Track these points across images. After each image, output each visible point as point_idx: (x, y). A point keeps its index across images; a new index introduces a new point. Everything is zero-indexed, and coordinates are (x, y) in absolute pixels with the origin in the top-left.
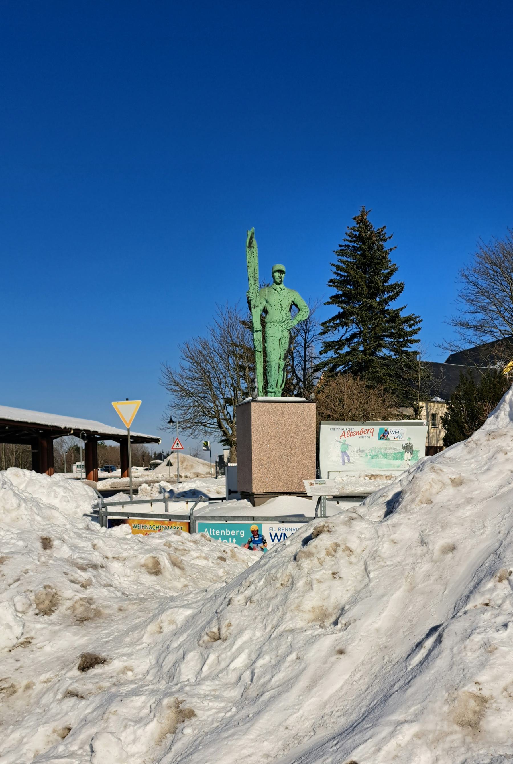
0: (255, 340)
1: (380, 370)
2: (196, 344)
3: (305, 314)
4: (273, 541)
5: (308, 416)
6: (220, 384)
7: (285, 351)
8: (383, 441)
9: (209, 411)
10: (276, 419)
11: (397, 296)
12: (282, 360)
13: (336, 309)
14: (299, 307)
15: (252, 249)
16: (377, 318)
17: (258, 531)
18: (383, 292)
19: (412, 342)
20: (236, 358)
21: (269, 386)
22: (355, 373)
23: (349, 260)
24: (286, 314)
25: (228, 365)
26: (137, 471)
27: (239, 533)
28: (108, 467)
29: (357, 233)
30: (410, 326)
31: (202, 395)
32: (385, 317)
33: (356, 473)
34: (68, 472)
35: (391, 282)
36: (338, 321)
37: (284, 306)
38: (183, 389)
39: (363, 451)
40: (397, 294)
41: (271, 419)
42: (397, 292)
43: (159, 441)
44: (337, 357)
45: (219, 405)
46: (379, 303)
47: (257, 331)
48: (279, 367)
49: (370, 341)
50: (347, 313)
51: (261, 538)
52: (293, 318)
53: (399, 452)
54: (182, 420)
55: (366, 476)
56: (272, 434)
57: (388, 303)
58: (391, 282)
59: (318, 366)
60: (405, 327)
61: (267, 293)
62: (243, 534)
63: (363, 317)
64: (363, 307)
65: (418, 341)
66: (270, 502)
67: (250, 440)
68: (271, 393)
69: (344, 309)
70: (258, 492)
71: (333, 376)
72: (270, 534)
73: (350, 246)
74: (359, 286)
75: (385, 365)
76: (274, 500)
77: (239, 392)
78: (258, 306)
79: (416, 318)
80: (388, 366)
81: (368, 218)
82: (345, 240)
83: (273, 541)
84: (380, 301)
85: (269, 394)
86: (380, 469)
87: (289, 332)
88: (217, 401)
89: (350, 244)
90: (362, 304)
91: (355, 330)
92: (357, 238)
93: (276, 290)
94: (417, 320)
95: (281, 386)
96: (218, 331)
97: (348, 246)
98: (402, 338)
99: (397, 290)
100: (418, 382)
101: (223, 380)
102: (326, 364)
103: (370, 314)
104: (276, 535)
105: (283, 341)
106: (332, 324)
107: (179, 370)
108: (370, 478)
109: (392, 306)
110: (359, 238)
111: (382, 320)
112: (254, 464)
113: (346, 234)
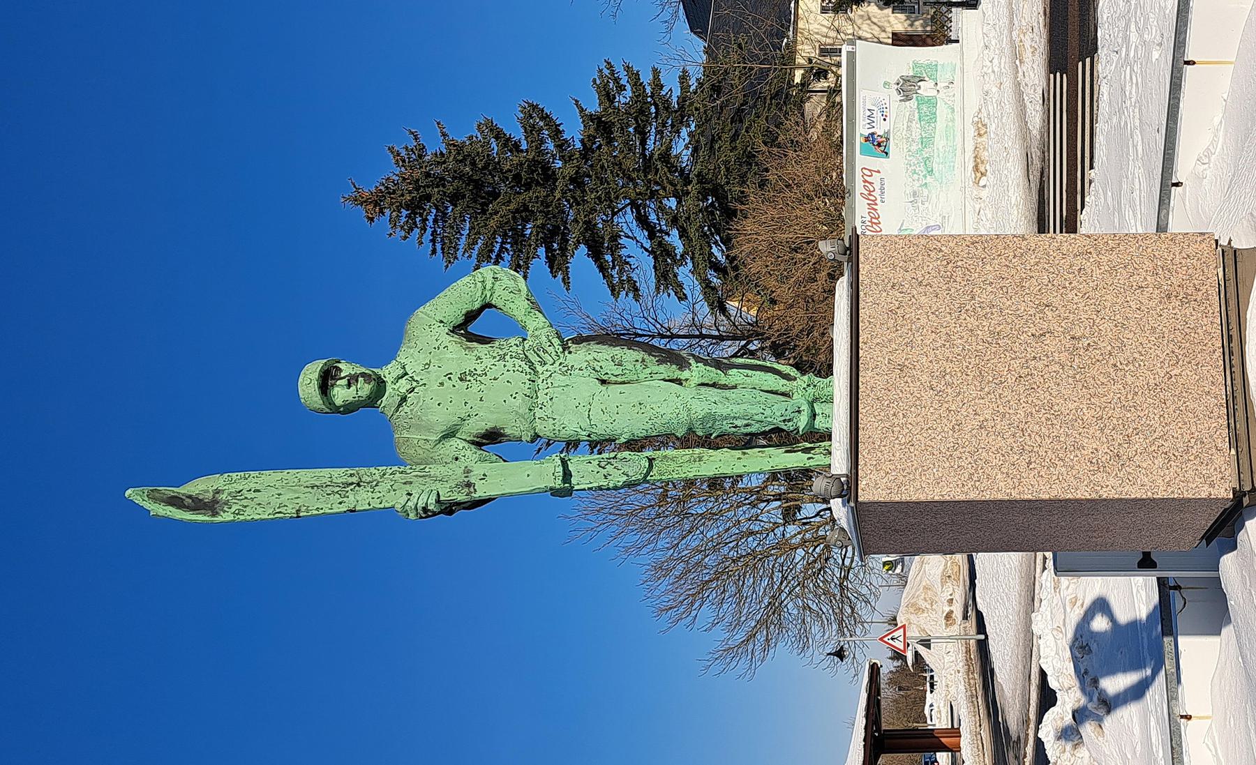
0: (604, 483)
2: (657, 593)
6: (752, 533)
12: (685, 374)
13: (580, 259)
14: (477, 305)
16: (602, 167)
18: (541, 153)
19: (658, 86)
20: (692, 496)
21: (789, 427)
22: (730, 214)
24: (503, 358)
25: (711, 516)
26: (935, 707)
29: (404, 212)
30: (621, 88)
32: (599, 147)
36: (608, 258)
37: (469, 364)
40: (545, 117)
41: (926, 421)
42: (542, 118)
44: (692, 259)
45: (800, 536)
47: (567, 475)
48: (714, 385)
49: (657, 183)
50: (588, 235)
52: (520, 331)
56: (987, 414)
57: (566, 141)
58: (518, 134)
59: (711, 305)
61: (415, 436)
63: (599, 198)
65: (656, 72)
70: (1230, 472)
71: (736, 268)
74: (526, 209)
75: (712, 147)
78: (467, 471)
80: (713, 141)
81: (369, 188)
85: (820, 423)
86: (959, 152)
87: (573, 347)
89: (429, 231)
90: (568, 201)
91: (630, 216)
93: (404, 399)
94: (606, 72)
96: (631, 539)
97: (434, 233)
98: (649, 108)
102: (707, 286)
106: (614, 273)
107: (720, 633)
109: (574, 131)
110: (415, 207)
112: (1111, 488)
113: (406, 238)
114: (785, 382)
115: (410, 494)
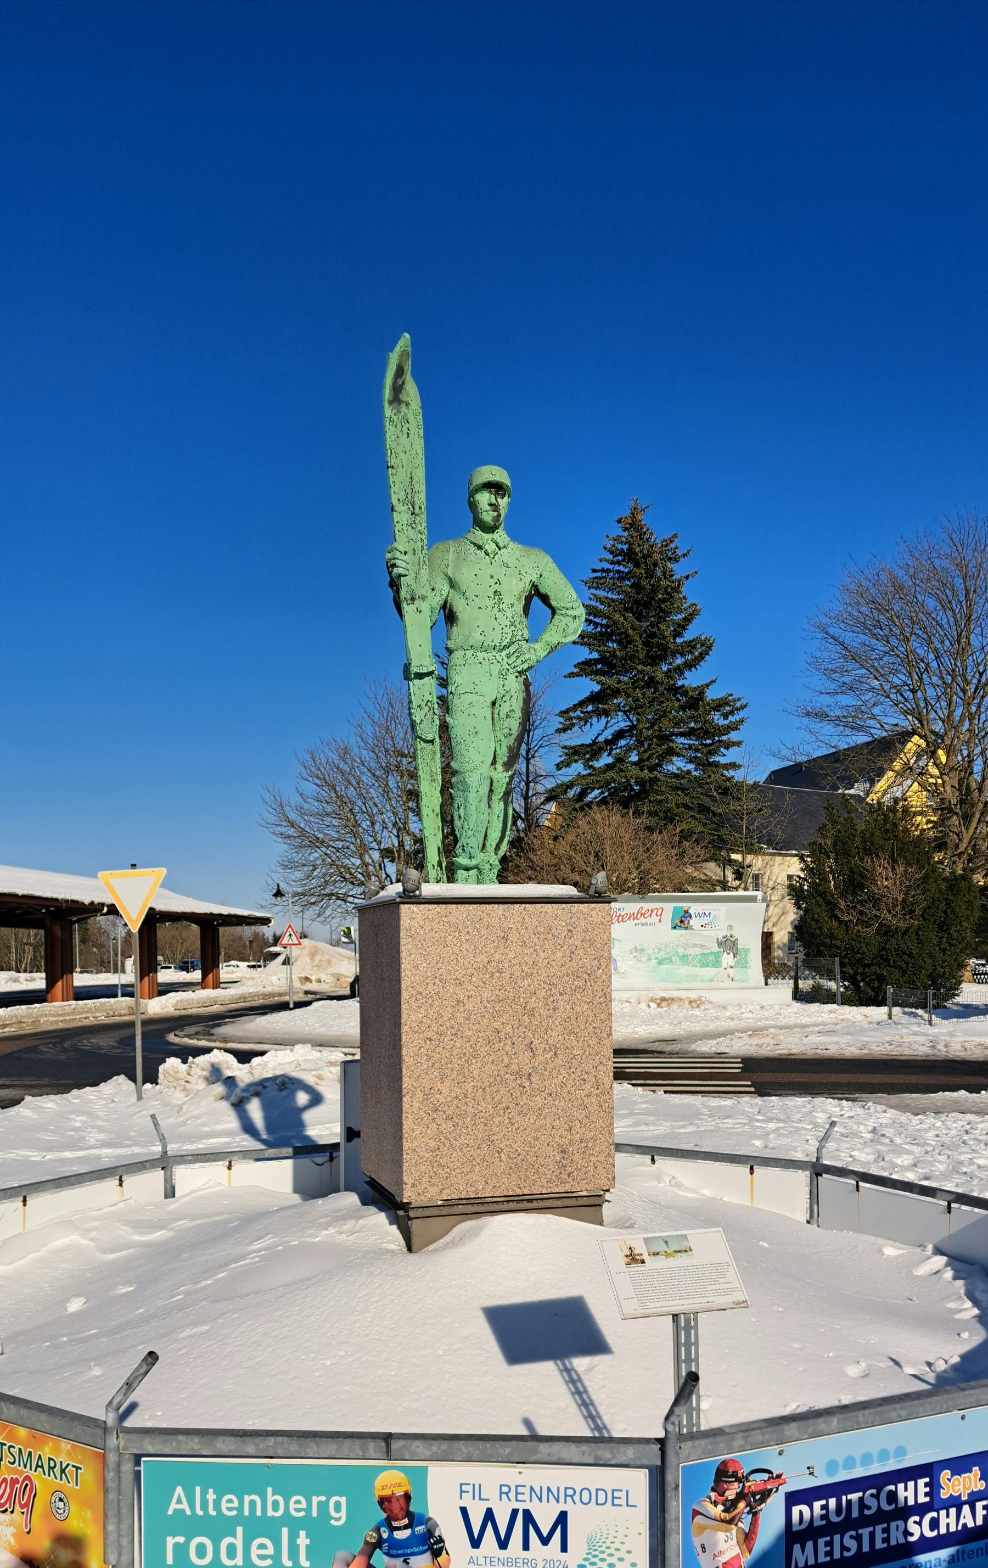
0: (415, 705)
1: (670, 797)
2: (326, 750)
3: (573, 626)
4: (476, 1543)
5: (586, 945)
6: (373, 824)
7: (511, 741)
8: (679, 932)
9: (351, 874)
10: (483, 958)
11: (700, 661)
12: (500, 767)
13: (589, 686)
14: (553, 603)
15: (403, 408)
16: (662, 702)
17: (407, 1497)
20: (402, 776)
21: (459, 850)
22: (625, 804)
23: (610, 595)
24: (513, 624)
26: (236, 969)
27: (323, 1506)
28: (187, 962)
29: (625, 547)
30: (725, 716)
31: (340, 844)
33: (631, 993)
34: (116, 971)
35: (689, 635)
36: (590, 708)
37: (508, 598)
38: (303, 833)
39: (642, 950)
40: (701, 657)
41: (464, 957)
42: (701, 654)
43: (270, 922)
44: (590, 775)
45: (370, 861)
46: (668, 674)
47: (420, 676)
48: (491, 790)
49: (649, 745)
51: (420, 1529)
53: (712, 953)
54: (300, 890)
55: (652, 1000)
56: (469, 1006)
57: (682, 674)
58: (689, 635)
59: (553, 790)
60: (716, 718)
61: (451, 556)
62: (343, 1513)
63: (638, 700)
64: (636, 681)
65: (739, 744)
66: (462, 1239)
67: (397, 1025)
68: (467, 869)
69: (603, 684)
70: (424, 1200)
71: (582, 809)
72: (464, 1511)
73: (611, 571)
74: (630, 642)
75: (678, 788)
76: (476, 1232)
77: (408, 838)
78: (423, 598)
79: (735, 700)
81: (644, 519)
82: (601, 560)
83: (476, 1543)
84: (669, 670)
85: (461, 874)
86: (677, 986)
87: (521, 679)
88: (367, 857)
89: (611, 567)
92: (624, 556)
93: (480, 548)
94: (738, 704)
95: (498, 847)
96: (369, 729)
97: (608, 571)
98: (710, 738)
99: (700, 651)
100: (742, 819)
101: (378, 818)
102: (570, 786)
103: (650, 692)
104: (489, 1516)
105: (505, 708)
106: (578, 713)
107: (295, 799)
108: (659, 1005)
109: (691, 680)
110: (629, 556)
111: (673, 704)
113: (605, 548)
114: (494, 846)
115: (406, 553)
